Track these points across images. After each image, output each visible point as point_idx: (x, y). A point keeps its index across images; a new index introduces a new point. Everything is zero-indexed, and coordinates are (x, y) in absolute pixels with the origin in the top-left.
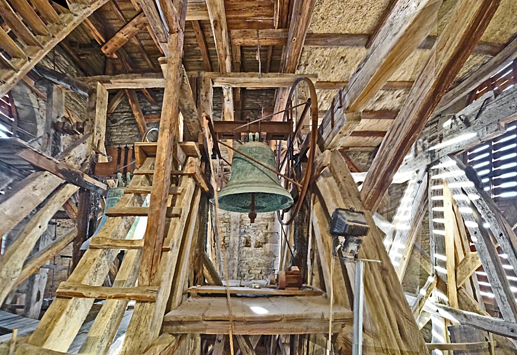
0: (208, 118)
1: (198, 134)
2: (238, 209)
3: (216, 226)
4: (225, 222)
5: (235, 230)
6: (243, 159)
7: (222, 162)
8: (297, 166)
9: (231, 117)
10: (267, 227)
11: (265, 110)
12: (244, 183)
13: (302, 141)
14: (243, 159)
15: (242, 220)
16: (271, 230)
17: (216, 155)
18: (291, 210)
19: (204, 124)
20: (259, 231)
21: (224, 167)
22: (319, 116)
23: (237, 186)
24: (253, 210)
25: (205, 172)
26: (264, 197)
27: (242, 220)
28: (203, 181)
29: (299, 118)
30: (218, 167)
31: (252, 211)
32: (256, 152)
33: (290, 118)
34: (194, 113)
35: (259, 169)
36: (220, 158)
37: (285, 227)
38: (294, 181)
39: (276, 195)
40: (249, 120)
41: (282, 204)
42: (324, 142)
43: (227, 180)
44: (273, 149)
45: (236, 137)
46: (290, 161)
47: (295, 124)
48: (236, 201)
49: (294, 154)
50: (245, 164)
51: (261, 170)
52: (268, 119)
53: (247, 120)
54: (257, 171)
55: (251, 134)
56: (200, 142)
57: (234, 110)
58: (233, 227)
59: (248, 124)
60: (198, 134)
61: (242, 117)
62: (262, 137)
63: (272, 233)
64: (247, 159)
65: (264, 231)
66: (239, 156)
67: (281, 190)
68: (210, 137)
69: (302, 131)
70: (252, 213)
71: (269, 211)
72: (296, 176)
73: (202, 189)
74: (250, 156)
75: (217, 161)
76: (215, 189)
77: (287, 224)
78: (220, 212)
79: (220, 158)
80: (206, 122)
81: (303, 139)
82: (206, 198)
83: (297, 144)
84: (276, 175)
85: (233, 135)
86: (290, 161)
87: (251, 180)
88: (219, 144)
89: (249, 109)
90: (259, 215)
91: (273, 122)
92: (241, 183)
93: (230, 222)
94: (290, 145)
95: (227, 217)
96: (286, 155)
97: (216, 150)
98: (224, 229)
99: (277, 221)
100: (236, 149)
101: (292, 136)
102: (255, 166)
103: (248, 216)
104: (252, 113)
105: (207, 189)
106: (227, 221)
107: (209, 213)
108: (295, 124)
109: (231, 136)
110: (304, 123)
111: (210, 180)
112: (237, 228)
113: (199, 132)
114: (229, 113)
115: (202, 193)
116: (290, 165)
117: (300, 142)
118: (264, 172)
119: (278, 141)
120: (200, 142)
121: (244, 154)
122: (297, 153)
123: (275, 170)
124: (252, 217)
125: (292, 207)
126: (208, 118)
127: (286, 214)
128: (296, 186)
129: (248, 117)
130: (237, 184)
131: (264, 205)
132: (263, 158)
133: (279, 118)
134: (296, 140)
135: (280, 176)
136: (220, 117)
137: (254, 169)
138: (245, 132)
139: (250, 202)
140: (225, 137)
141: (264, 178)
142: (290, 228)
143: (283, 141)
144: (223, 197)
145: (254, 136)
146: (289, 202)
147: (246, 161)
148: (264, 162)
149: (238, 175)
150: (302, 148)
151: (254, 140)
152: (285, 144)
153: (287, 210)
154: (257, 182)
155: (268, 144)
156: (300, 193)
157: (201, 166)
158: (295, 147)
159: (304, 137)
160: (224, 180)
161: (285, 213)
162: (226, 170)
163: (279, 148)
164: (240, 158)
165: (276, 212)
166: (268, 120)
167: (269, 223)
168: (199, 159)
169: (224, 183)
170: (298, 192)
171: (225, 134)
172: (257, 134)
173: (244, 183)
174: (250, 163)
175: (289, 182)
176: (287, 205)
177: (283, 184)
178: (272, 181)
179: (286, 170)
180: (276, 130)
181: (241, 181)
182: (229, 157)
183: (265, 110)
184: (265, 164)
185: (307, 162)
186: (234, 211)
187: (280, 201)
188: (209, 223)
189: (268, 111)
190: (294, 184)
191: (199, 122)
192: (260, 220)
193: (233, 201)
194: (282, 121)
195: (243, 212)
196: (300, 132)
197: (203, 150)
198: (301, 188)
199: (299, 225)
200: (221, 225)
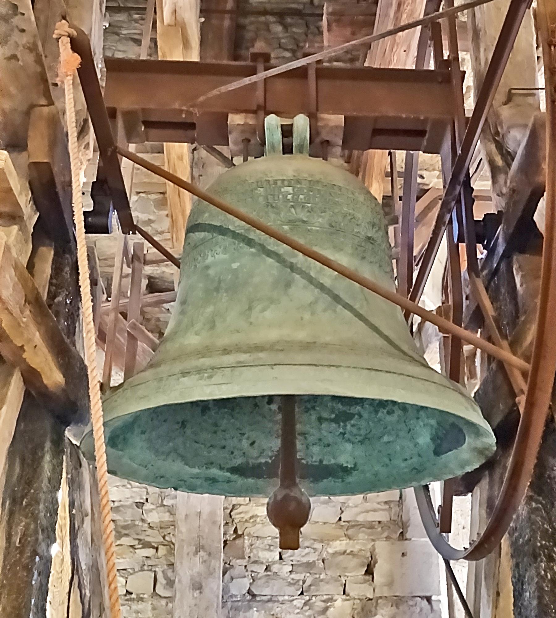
0: (80, 45)
1: (28, 113)
2: (213, 480)
3: (95, 568)
4: (147, 545)
5: (198, 587)
6: (235, 235)
7: (139, 247)
8: (495, 272)
9: (186, 44)
10: (369, 572)
11: (337, 18)
12: (238, 349)
13: (508, 157)
14: (235, 235)
15: (238, 536)
16: (390, 584)
17: (107, 214)
18: (485, 483)
19: (62, 70)
20: (326, 589)
21: (148, 270)
22: (425, 68)
23: (206, 362)
24: (289, 480)
25: (52, 296)
26: (343, 418)
27: (238, 536)
28: (37, 338)
29: (487, 55)
30: (119, 270)
31: (283, 486)
32: (296, 204)
33: (446, 54)
34: (16, 21)
35: (311, 280)
36: (129, 226)
37: (462, 570)
38: (489, 339)
39: (404, 407)
40: (266, 57)
41: (437, 453)
42: (455, 204)
43: (161, 334)
44: (378, 189)
45: (206, 131)
46: (463, 247)
47: (469, 81)
48: (205, 436)
49: (478, 216)
50: (244, 260)
51: (322, 287)
52: (352, 56)
53: (255, 57)
54: (302, 293)
55: (272, 122)
56: (38, 150)
57: (203, 12)
58: (188, 568)
59: (262, 75)
60: (28, 113)
61: (237, 43)
62: (325, 136)
63: (398, 601)
64: (255, 234)
65: (354, 591)
66: (217, 218)
67: (424, 383)
68: (82, 132)
69: (506, 112)
70: (286, 498)
71: (374, 485)
72: (497, 321)
73: (31, 377)
74: (271, 221)
75: (113, 242)
76: (95, 377)
77: (475, 553)
78: (119, 491)
79: (129, 226)
80: (68, 60)
81: (511, 146)
82: (47, 424)
83: (486, 169)
84: (400, 314)
85: (192, 126)
86: (463, 247)
87: (273, 335)
88: (125, 163)
89: (265, 13)
90: (323, 510)
91: (370, 69)
92: (226, 351)
93: (170, 546)
94: (455, 176)
95: (154, 517)
96: (440, 219)
97: (108, 189)
98: (141, 583)
99: (420, 540)
100: (203, 186)
101: (461, 133)
102: (292, 267)
103: (263, 511)
104: (278, 28)
105: (54, 378)
106: (154, 537)
107: (63, 495)
108: (469, 81)
109: (183, 128)
110: (509, 78)
111: (72, 331)
112: (211, 573)
113: (32, 106)
114: (179, 25)
115: (27, 395)
116: (464, 266)
117: (499, 162)
118: (337, 299)
119: (400, 155)
120: (38, 150)
121: (242, 210)
122: (493, 210)
123: (393, 287)
124: (289, 521)
125: (490, 465)
126: (80, 45)
127: (463, 505)
128: (501, 365)
129: (259, 47)
130: (205, 351)
131: (345, 460)
132: (334, 230)
133: (403, 53)
134: (480, 149)
135: (417, 319)
136: (138, 42)
137: (288, 285)
138: (246, 111)
139: (276, 444)
140: (153, 132)
141: (337, 326)
142: (493, 576)
143: (422, 157)
144: (137, 417)
145: (287, 131)
146: (469, 441)
147: (250, 242)
148: (338, 248)
149: (210, 309)
150: (513, 191)
151: (288, 149)
152: (432, 172)
153: (467, 483)
154: (307, 346)
155: (356, 168)
156: (522, 400)
157: (31, 266)
158: (481, 183)
159: (517, 140)
160: (141, 335)
161: (456, 499)
162: (154, 287)
163: (407, 185)
164: (222, 231)
165: (410, 493)
166: (352, 60)
167: (382, 549)
168: (23, 229)
169: (141, 345)
170: (513, 395)
171: (154, 119)
172: (301, 122)
173: (238, 349)
174: (270, 254)
175: (467, 348)
176: (465, 458)
177: (434, 357)
178: (380, 342)
179: (445, 288)
180: (390, 106)
181: (224, 341)
182: (173, 222)
183: (337, 18)
184: (343, 259)
185: (539, 252)
186: (192, 489)
187: (424, 439)
188: (59, 551)
189: (352, 24)
190: (490, 358)
191: (39, 61)
192: (329, 530)
193: (196, 437)
194: (411, 65)
195: (238, 493)
196: (497, 115)
197: (49, 190)
198: (524, 374)
199: (535, 556)
200: (123, 559)
